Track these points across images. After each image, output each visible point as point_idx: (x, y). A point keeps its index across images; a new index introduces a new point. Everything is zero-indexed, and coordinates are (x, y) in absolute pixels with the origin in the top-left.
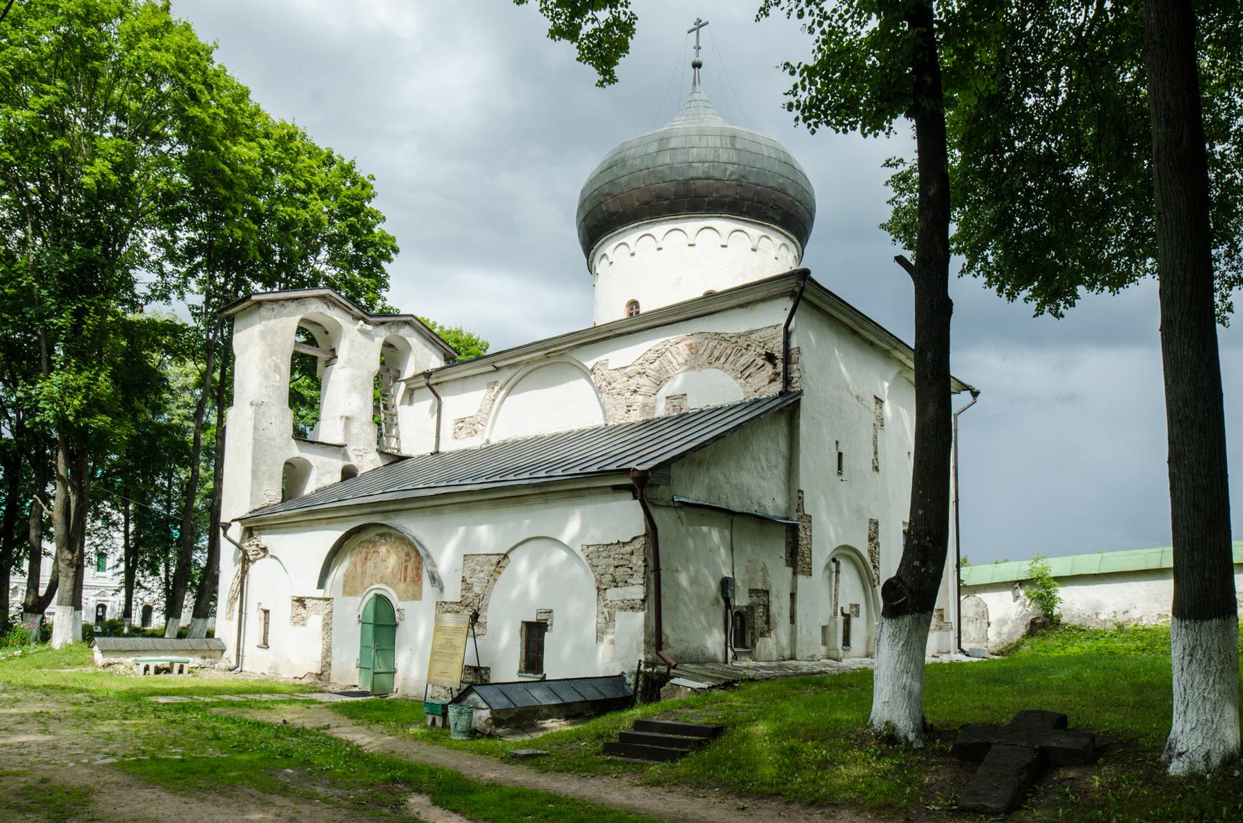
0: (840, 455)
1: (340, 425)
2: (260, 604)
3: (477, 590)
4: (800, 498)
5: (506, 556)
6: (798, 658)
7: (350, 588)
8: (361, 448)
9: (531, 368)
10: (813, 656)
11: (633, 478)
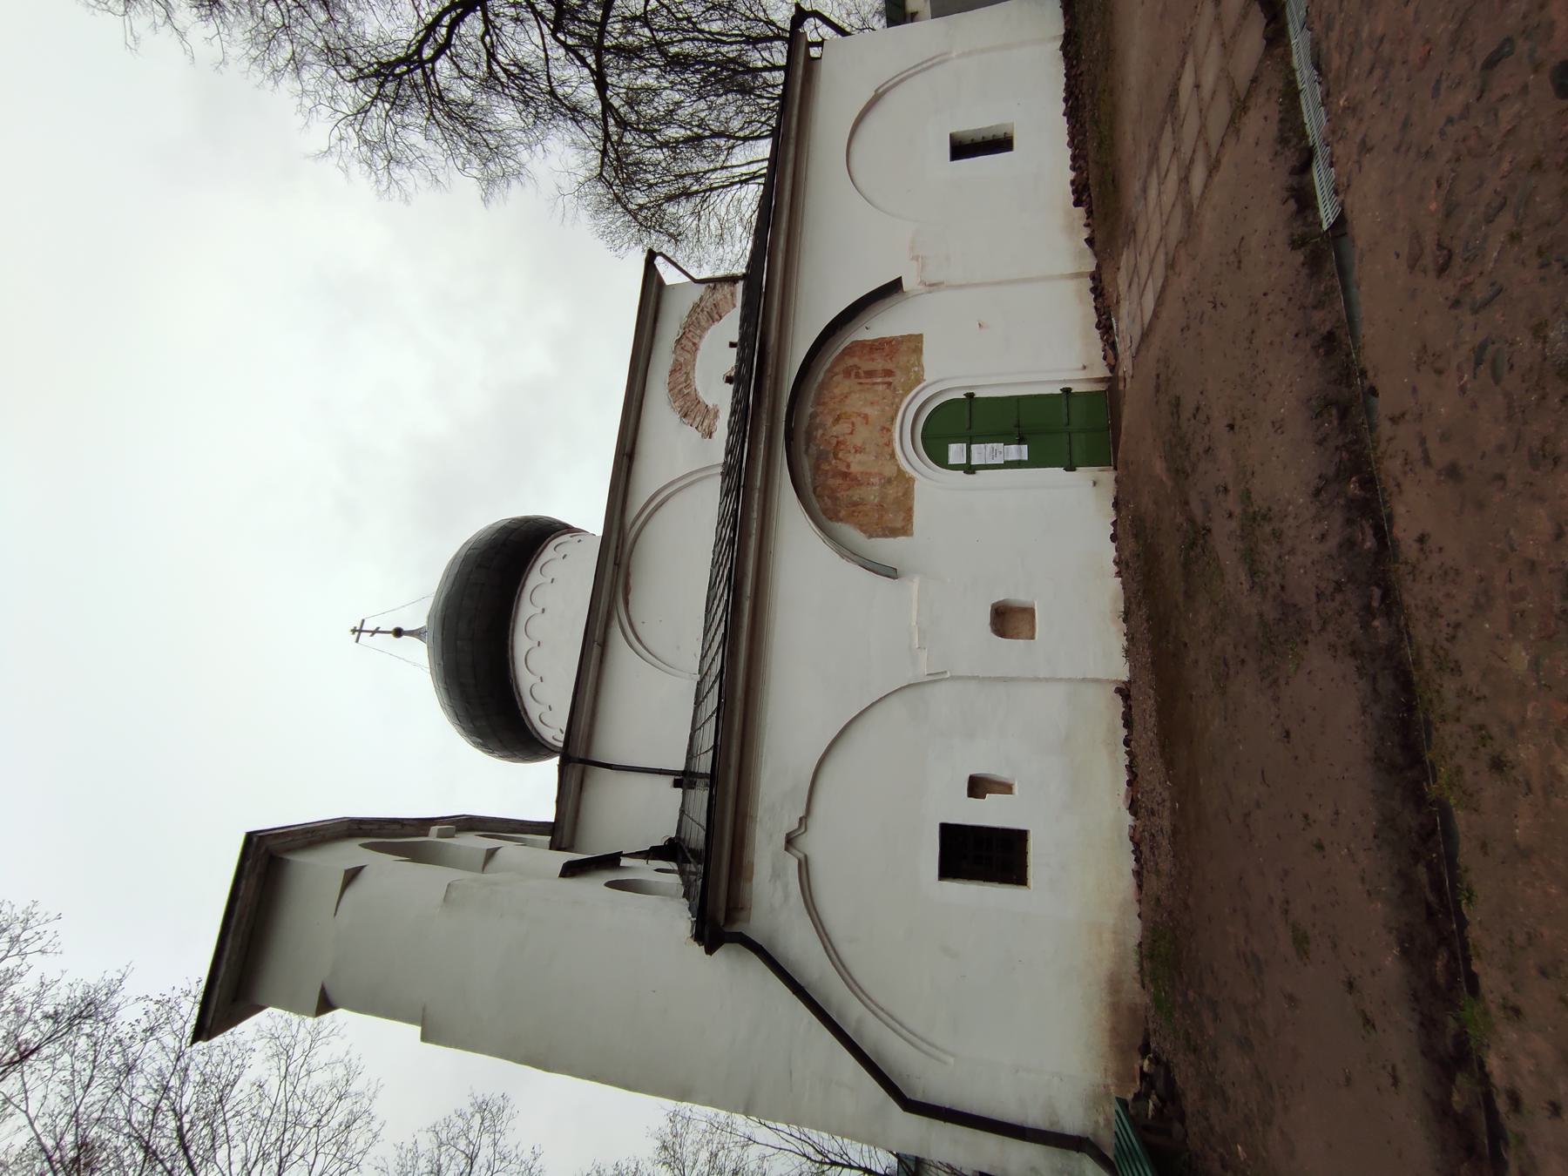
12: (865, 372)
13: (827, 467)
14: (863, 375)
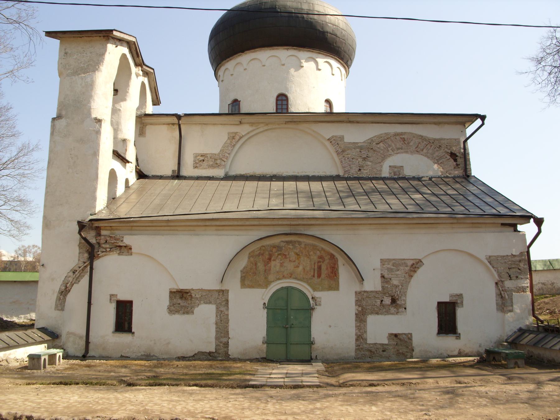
2: (112, 296)
14: (319, 264)
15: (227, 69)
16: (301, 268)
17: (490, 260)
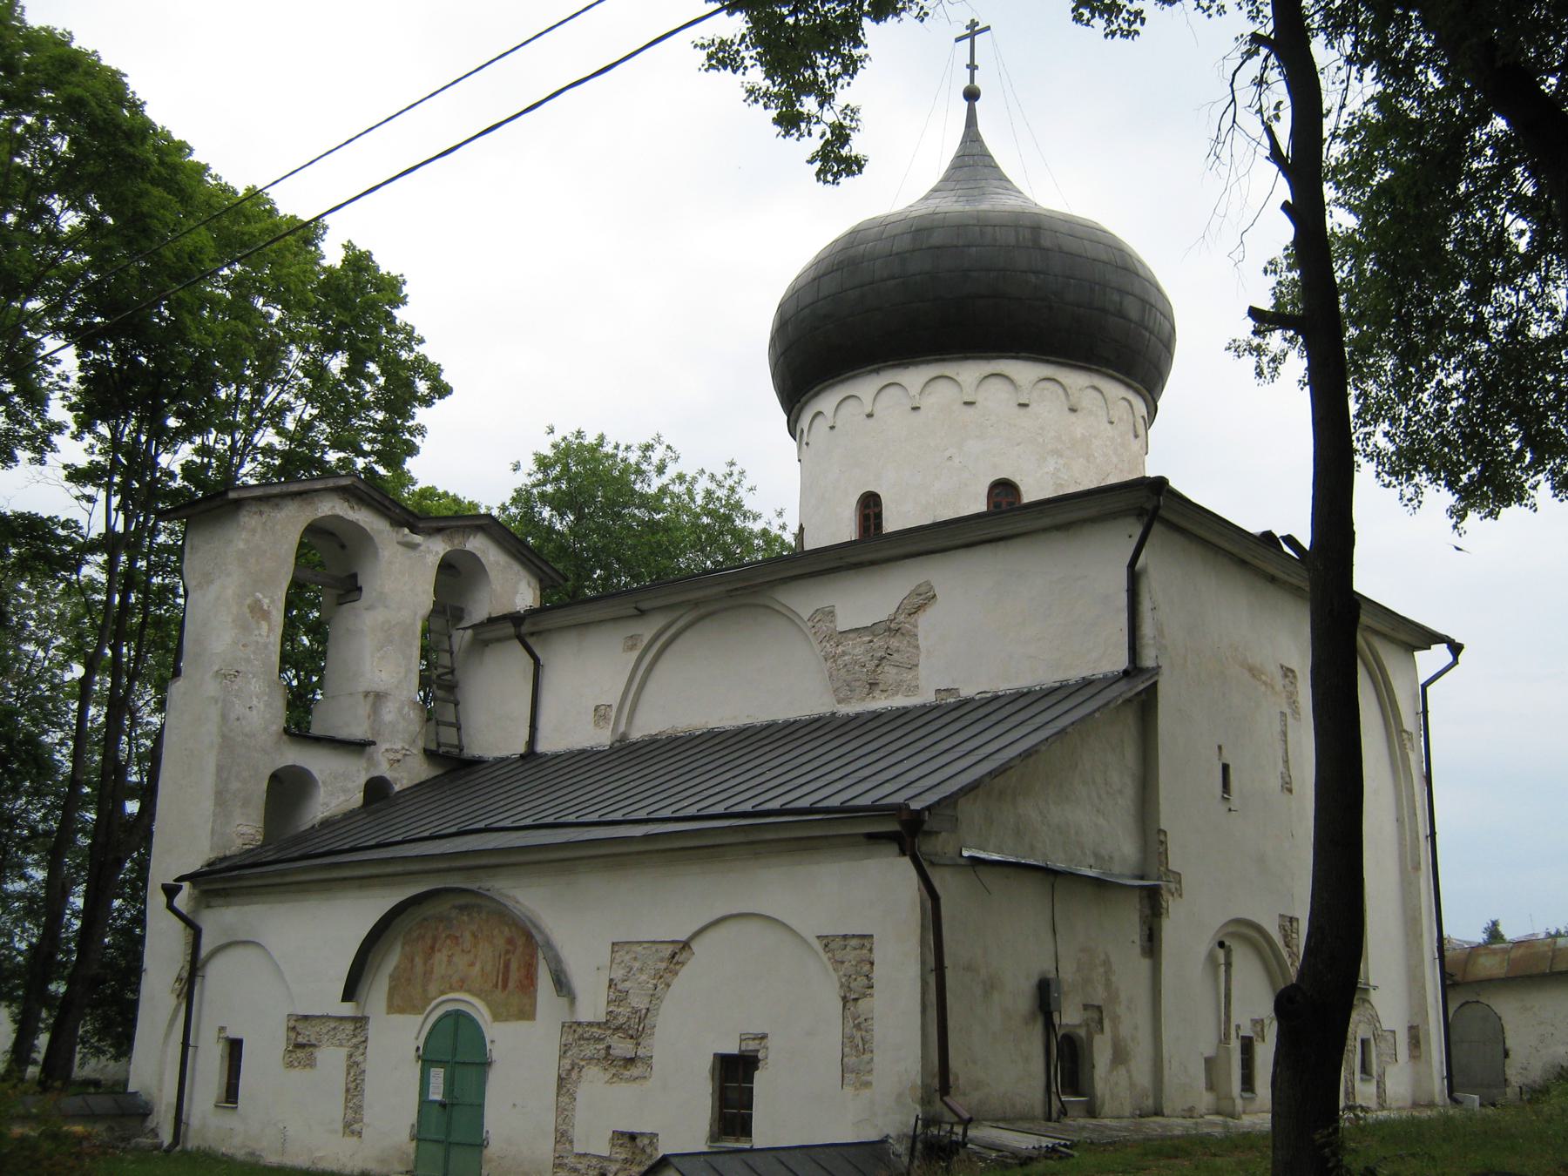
0: (1226, 768)
1: (364, 709)
2: (222, 1029)
3: (638, 1001)
4: (1162, 842)
5: (686, 945)
6: (1166, 1111)
7: (400, 1003)
8: (398, 746)
9: (702, 611)
10: (1191, 1109)
11: (902, 823)
12: (509, 960)
13: (441, 928)
14: (508, 957)
15: (819, 413)
16: (477, 967)
17: (827, 941)
